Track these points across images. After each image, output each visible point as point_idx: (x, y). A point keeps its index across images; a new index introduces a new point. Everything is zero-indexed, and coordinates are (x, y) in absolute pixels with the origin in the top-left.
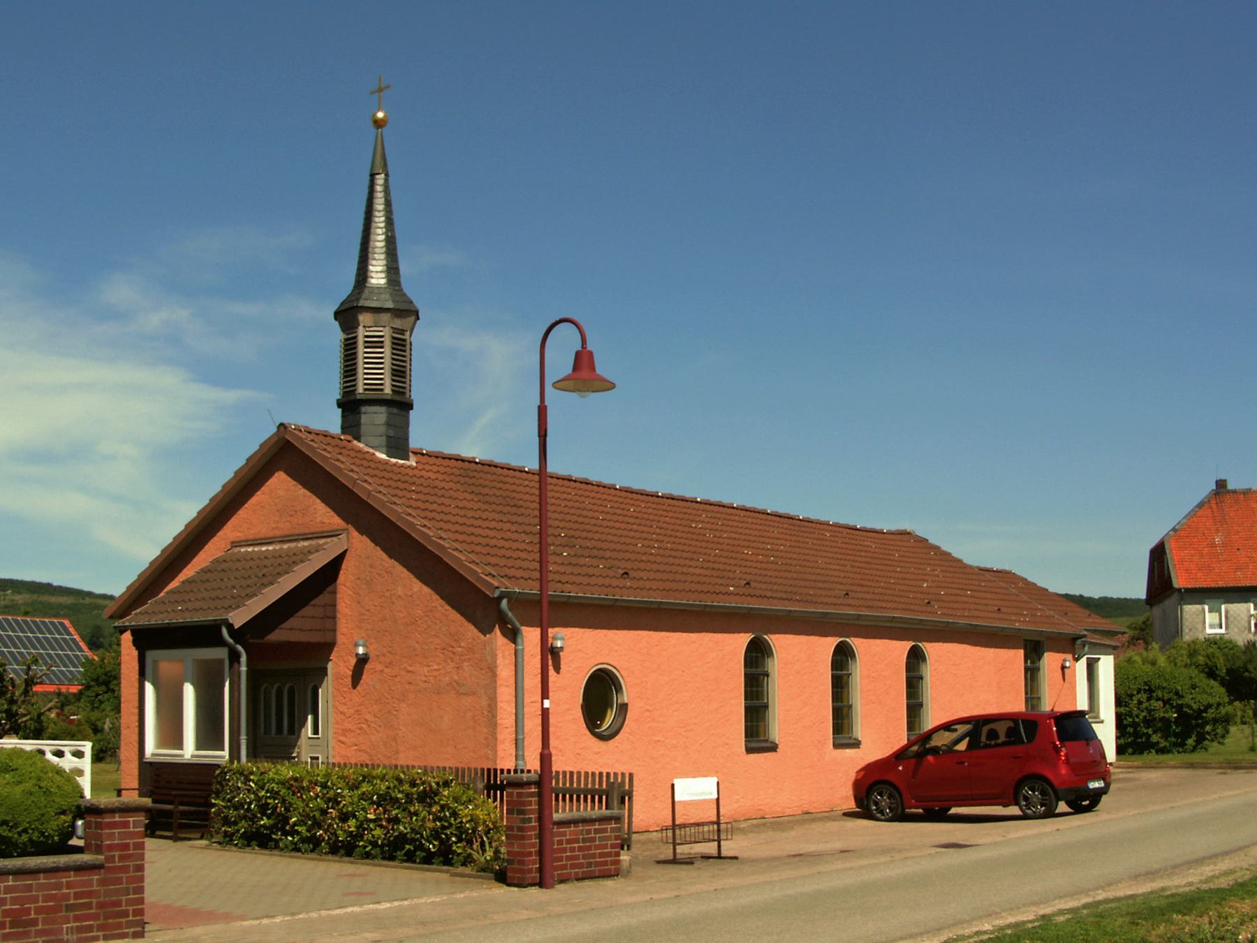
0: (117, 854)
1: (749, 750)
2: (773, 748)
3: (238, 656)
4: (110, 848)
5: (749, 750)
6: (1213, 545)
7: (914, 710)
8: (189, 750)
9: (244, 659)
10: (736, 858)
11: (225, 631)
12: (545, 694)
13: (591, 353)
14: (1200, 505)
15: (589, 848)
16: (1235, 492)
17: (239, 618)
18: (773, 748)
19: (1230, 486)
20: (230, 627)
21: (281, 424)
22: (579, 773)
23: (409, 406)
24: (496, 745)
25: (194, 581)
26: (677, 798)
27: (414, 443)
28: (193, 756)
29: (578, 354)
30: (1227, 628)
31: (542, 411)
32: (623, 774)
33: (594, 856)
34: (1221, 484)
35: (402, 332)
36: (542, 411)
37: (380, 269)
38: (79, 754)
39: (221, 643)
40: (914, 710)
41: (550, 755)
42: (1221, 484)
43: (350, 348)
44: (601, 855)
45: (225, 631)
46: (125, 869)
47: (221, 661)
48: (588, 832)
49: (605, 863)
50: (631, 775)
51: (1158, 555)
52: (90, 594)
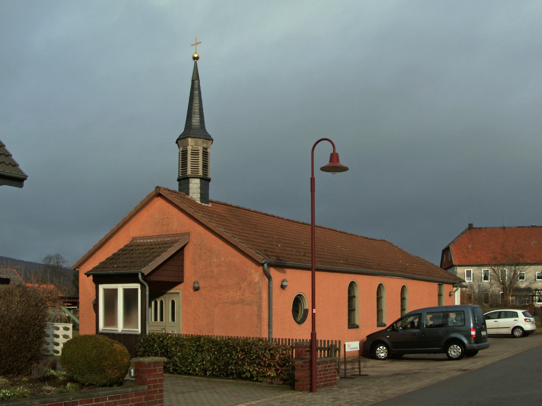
0: (152, 385)
1: (349, 328)
2: (357, 327)
3: (145, 287)
4: (150, 382)
5: (349, 328)
6: (468, 248)
7: (403, 309)
8: (120, 327)
9: (147, 288)
10: (368, 375)
11: (140, 276)
12: (313, 307)
13: (337, 154)
14: (463, 233)
15: (326, 374)
16: (476, 228)
17: (146, 270)
18: (357, 327)
19: (474, 226)
20: (143, 274)
21: (157, 187)
22: (325, 341)
23: (209, 180)
24: (261, 327)
25: (119, 255)
26: (346, 350)
27: (211, 197)
28: (122, 331)
29: (332, 155)
30: (473, 280)
31: (313, 180)
32: (336, 341)
33: (327, 377)
34: (471, 226)
35: (206, 149)
36: (313, 180)
37: (196, 119)
38: (66, 329)
39: (137, 281)
40: (403, 309)
41: (315, 334)
42: (471, 226)
43: (184, 155)
44: (331, 377)
45: (140, 276)
46: (155, 392)
47: (137, 289)
48: (326, 367)
49: (331, 380)
50: (340, 341)
51: (446, 251)
52: (425, 260)
